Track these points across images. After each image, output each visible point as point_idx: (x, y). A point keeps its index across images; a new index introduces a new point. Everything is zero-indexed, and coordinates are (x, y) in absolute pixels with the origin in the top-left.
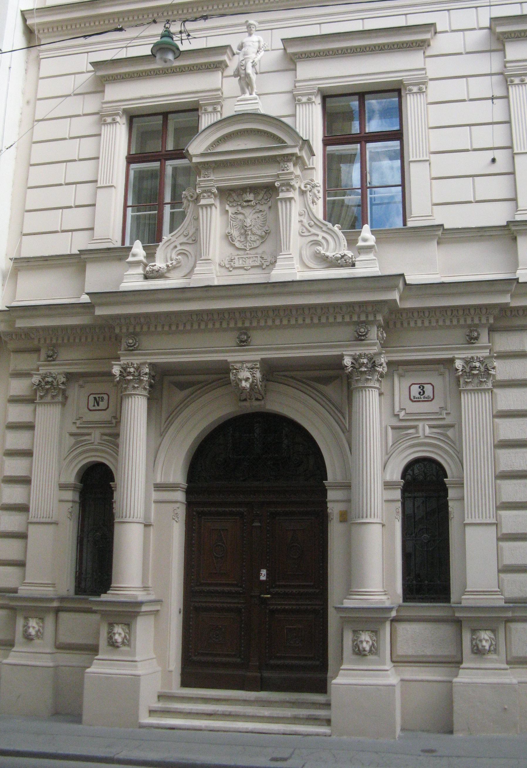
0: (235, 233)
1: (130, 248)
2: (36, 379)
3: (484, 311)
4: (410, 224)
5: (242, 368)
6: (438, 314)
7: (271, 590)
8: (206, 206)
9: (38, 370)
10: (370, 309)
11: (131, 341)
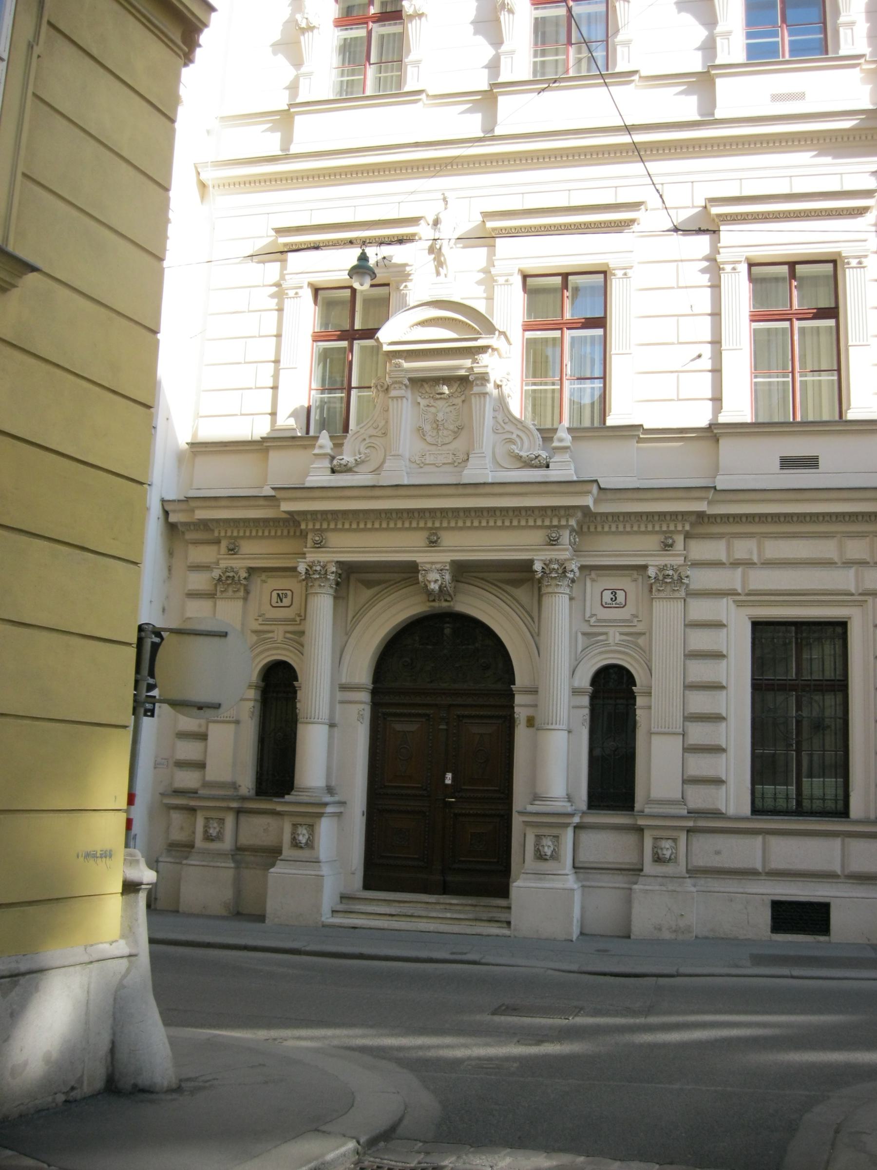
0: (427, 427)
1: (316, 438)
2: (216, 574)
3: (680, 518)
4: (610, 422)
5: (431, 570)
6: (633, 518)
7: (457, 794)
8: (397, 398)
9: (217, 563)
10: (562, 512)
11: (317, 538)
